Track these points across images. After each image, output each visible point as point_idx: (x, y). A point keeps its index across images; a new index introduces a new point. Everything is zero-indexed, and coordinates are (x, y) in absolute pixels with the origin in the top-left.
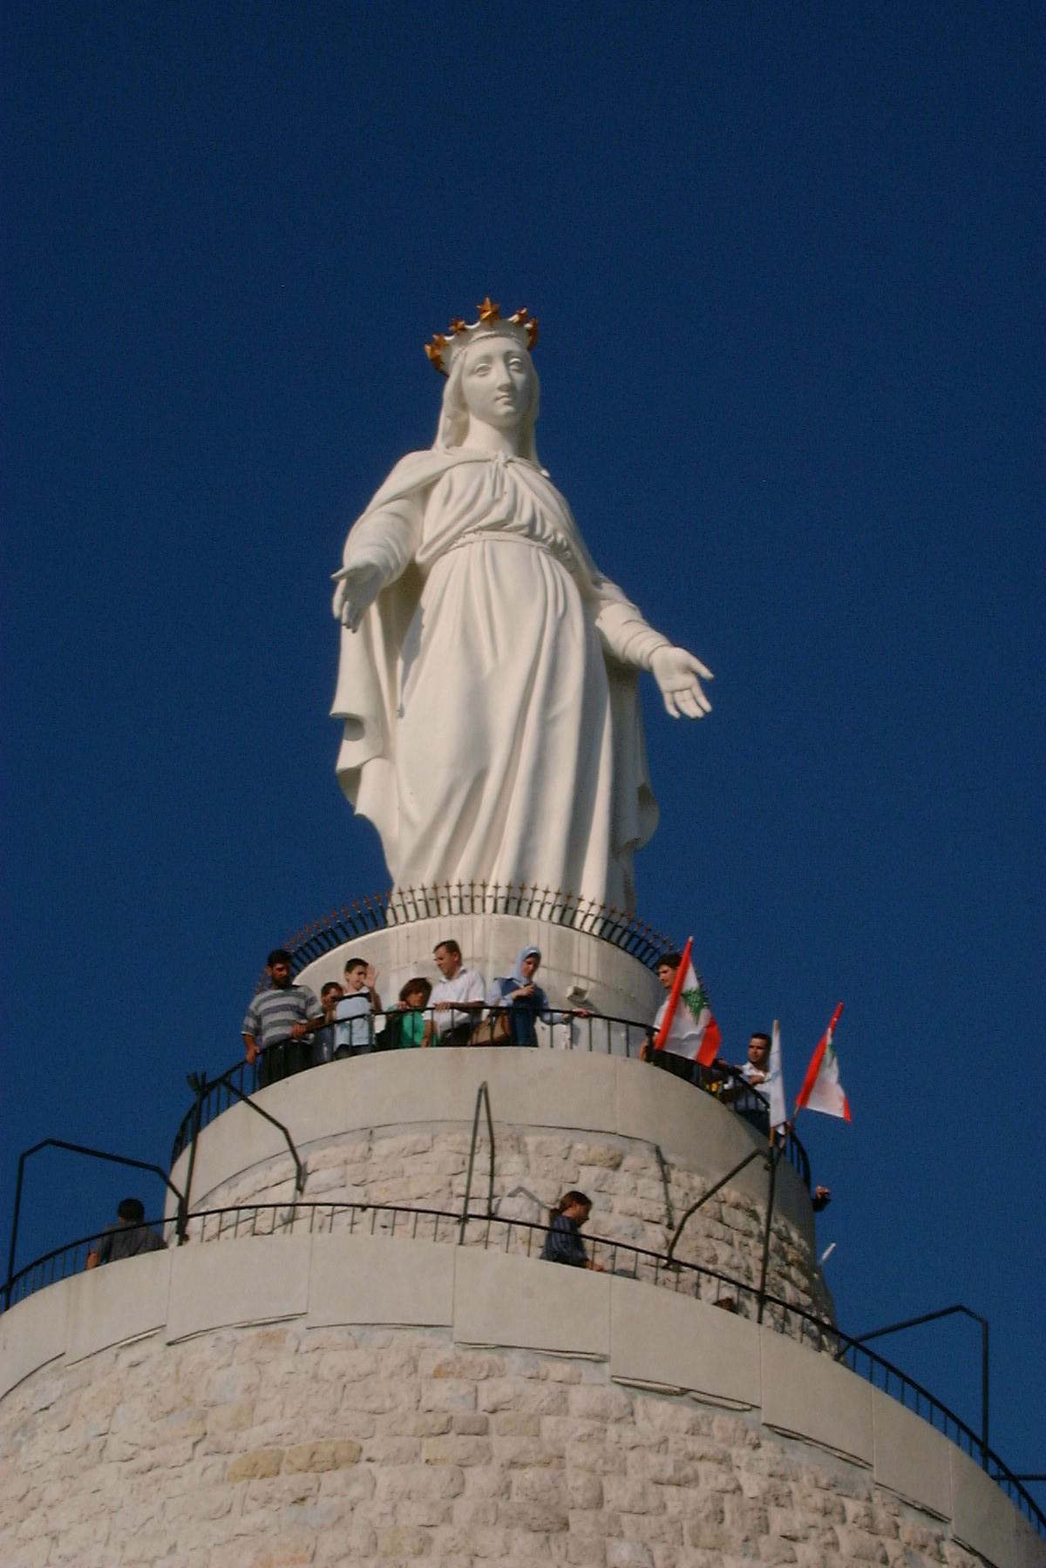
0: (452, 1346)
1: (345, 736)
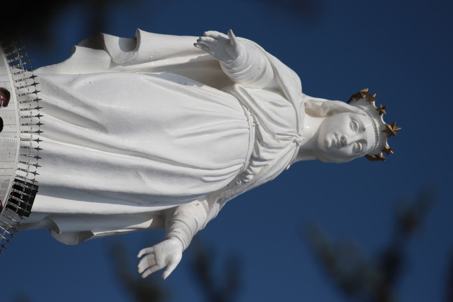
1: (120, 38)
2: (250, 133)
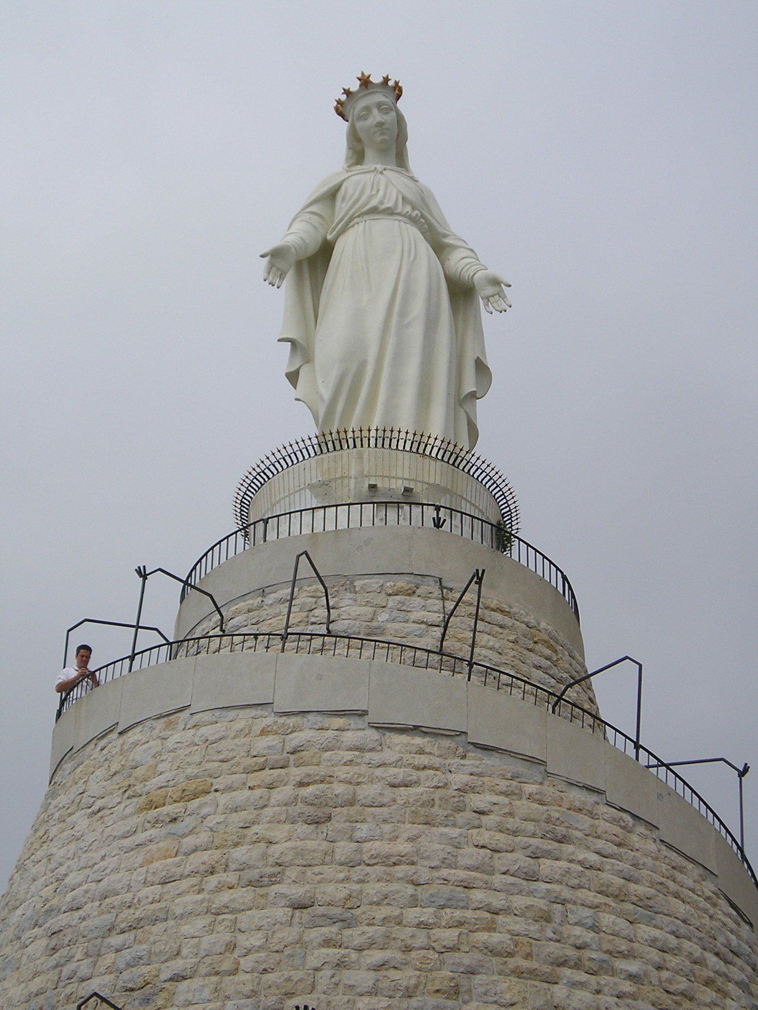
0: (273, 715)
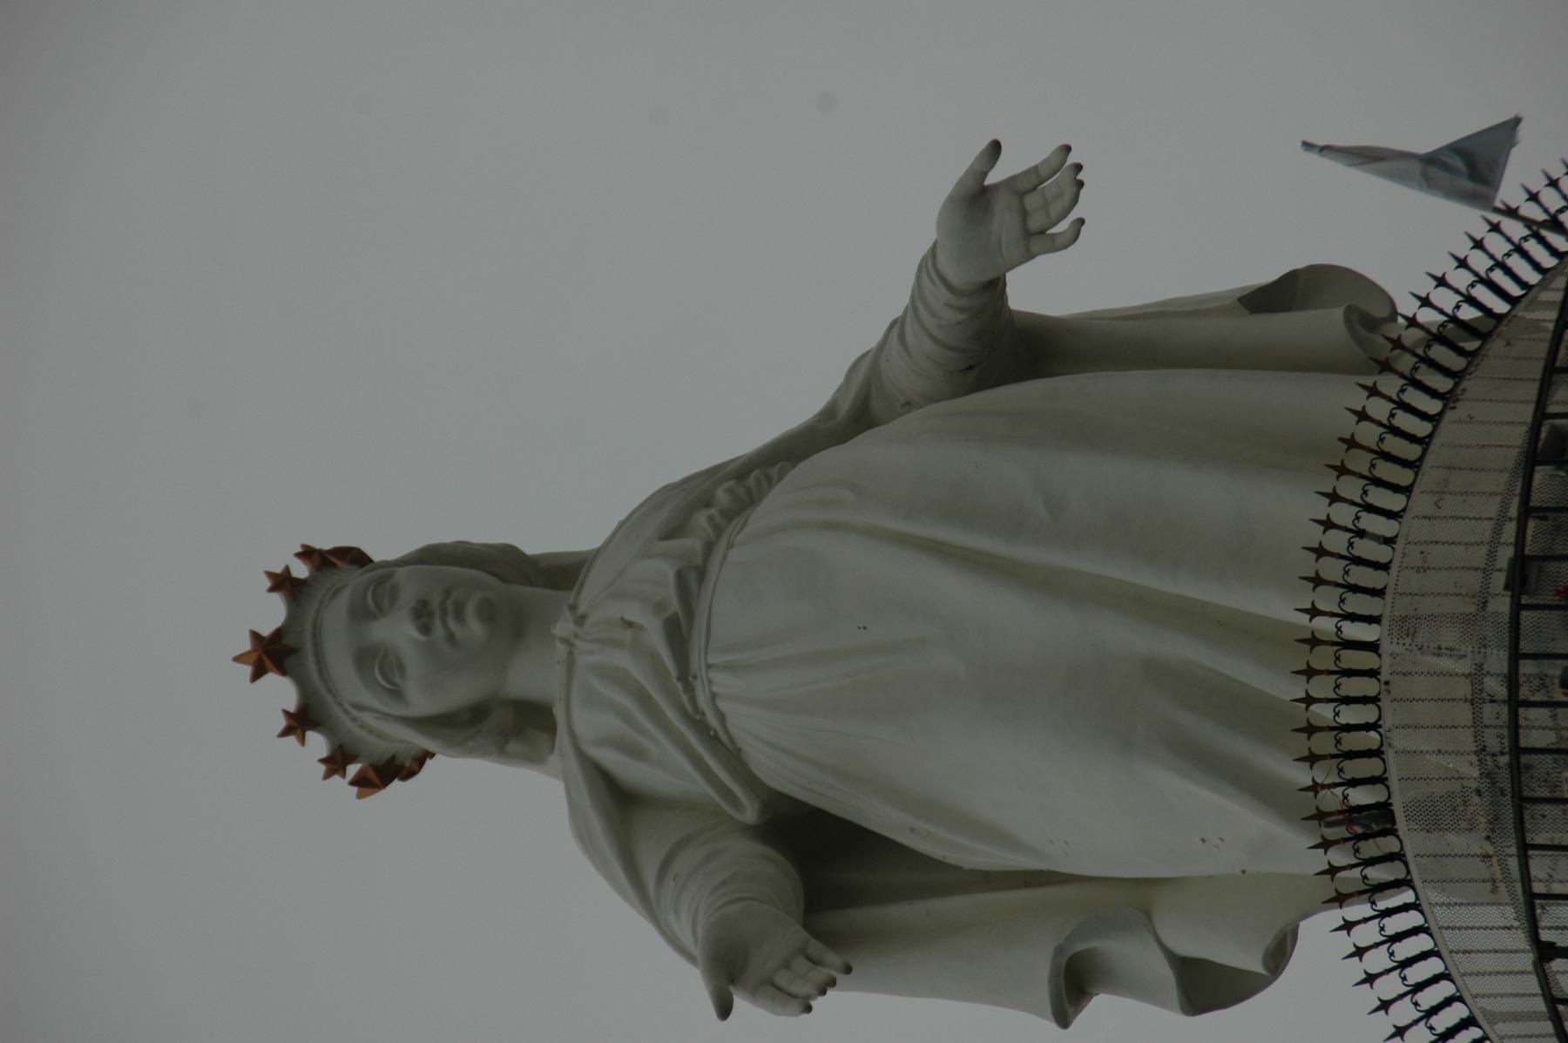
2: (706, 653)
